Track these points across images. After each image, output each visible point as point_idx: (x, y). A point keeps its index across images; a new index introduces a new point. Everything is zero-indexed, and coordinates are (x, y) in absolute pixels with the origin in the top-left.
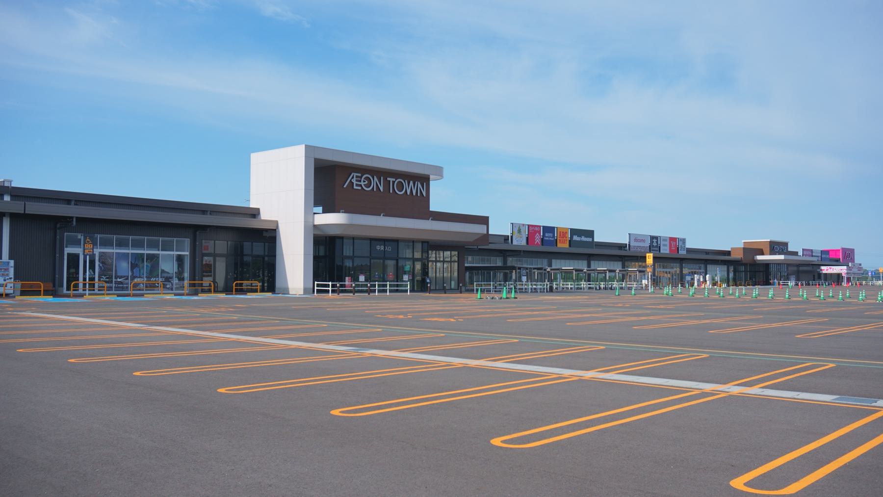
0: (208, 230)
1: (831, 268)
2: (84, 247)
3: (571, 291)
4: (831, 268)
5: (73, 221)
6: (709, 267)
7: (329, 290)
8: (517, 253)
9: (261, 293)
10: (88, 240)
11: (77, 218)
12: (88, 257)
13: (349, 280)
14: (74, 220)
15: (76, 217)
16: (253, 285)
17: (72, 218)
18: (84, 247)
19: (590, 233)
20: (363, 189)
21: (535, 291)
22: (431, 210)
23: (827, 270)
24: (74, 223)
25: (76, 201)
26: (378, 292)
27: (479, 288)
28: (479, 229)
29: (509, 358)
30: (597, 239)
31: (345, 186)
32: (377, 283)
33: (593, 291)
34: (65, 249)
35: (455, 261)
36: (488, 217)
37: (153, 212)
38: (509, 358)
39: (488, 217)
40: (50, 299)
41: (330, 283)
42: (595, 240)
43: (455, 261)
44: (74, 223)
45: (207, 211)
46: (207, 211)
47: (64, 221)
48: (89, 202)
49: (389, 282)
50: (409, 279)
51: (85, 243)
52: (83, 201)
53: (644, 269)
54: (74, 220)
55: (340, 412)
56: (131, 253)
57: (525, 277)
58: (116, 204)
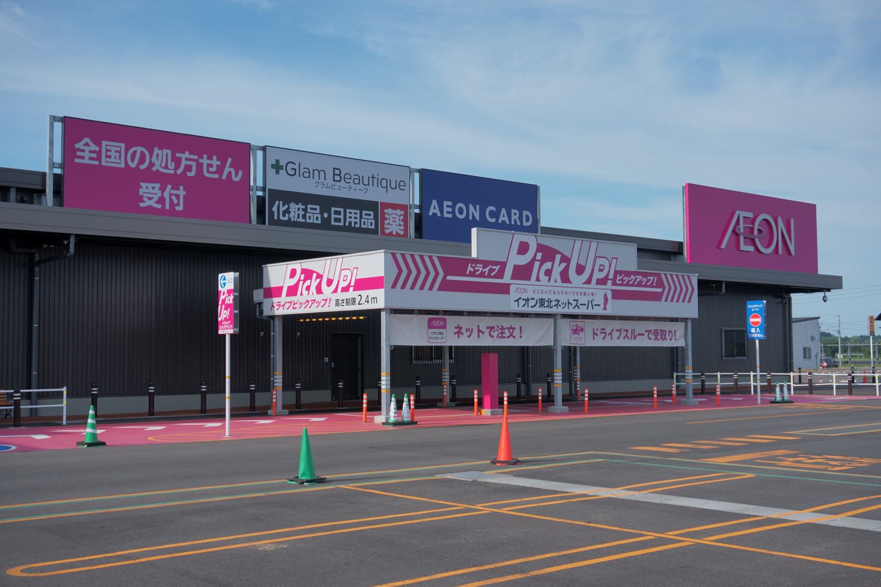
0: (765, 314)
1: (308, 274)
4: (308, 274)
12: (852, 355)
13: (236, 331)
15: (77, 236)
17: (67, 236)
20: (761, 252)
22: (472, 229)
23: (293, 291)
29: (441, 514)
31: (723, 246)
32: (719, 373)
33: (829, 398)
38: (441, 514)
41: (719, 374)
49: (721, 372)
53: (602, 331)
54: (72, 241)
55: (22, 571)
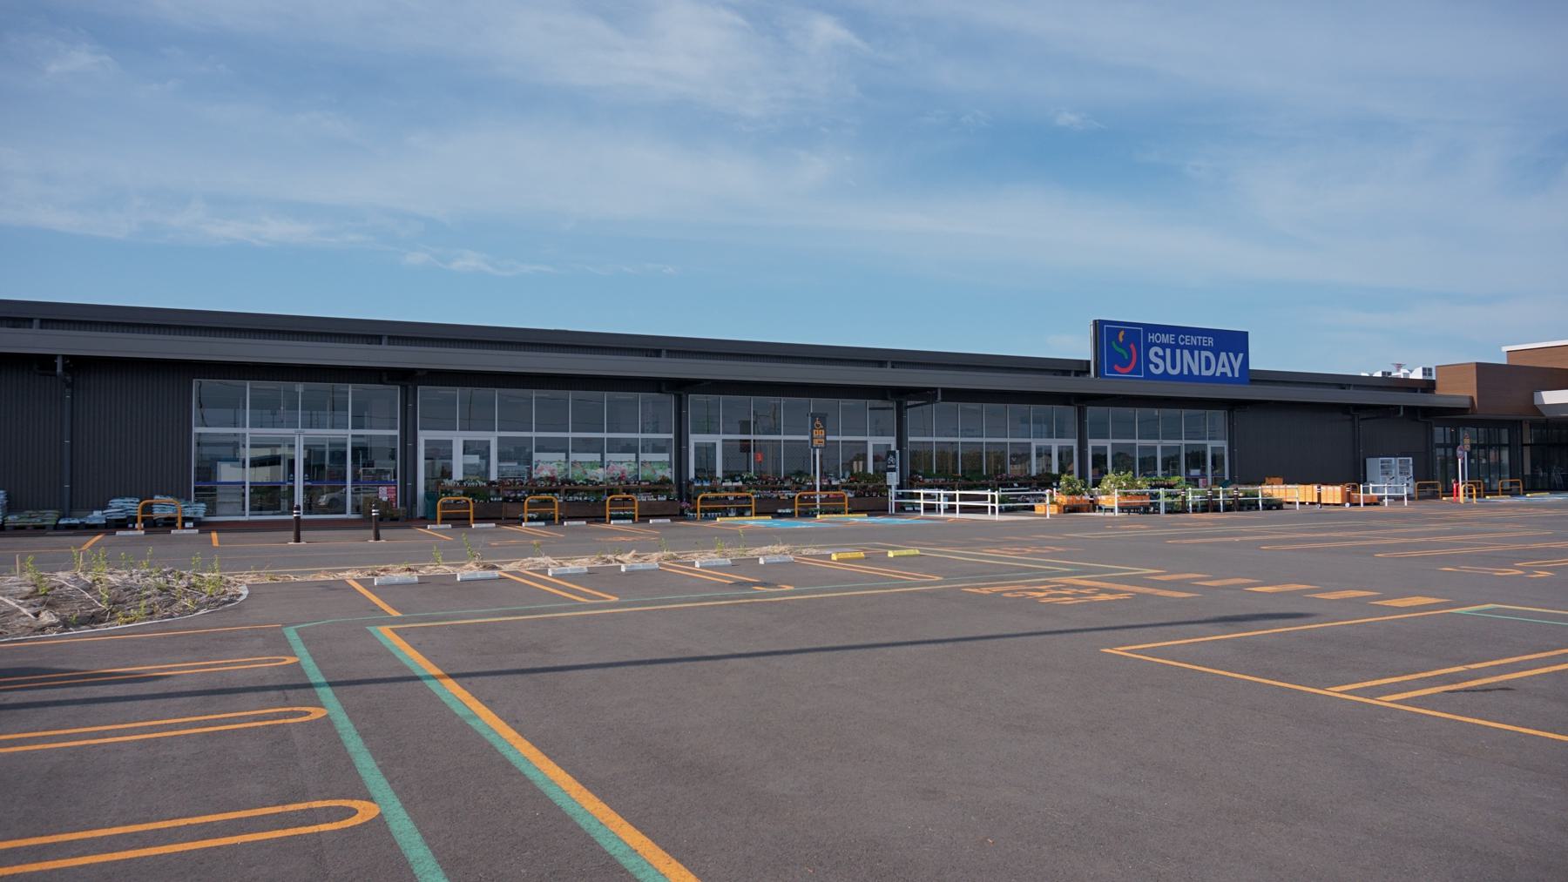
2: (812, 435)
3: (1397, 509)
5: (937, 393)
6: (1092, 411)
7: (955, 505)
8: (1453, 416)
9: (757, 518)
10: (818, 422)
11: (1405, 407)
12: (818, 451)
14: (1402, 409)
16: (1394, 490)
18: (812, 435)
19: (1236, 342)
21: (1209, 506)
24: (1402, 413)
25: (893, 362)
26: (925, 509)
27: (1371, 493)
28: (1224, 365)
30: (1261, 359)
34: (691, 436)
35: (1440, 446)
36: (1246, 334)
37: (566, 355)
39: (1246, 334)
40: (765, 522)
42: (1255, 364)
43: (1440, 446)
44: (1402, 413)
45: (886, 362)
46: (886, 362)
47: (925, 394)
48: (824, 359)
50: (535, 480)
51: (813, 428)
52: (524, 343)
56: (608, 439)
57: (1526, 474)
58: (123, 324)
